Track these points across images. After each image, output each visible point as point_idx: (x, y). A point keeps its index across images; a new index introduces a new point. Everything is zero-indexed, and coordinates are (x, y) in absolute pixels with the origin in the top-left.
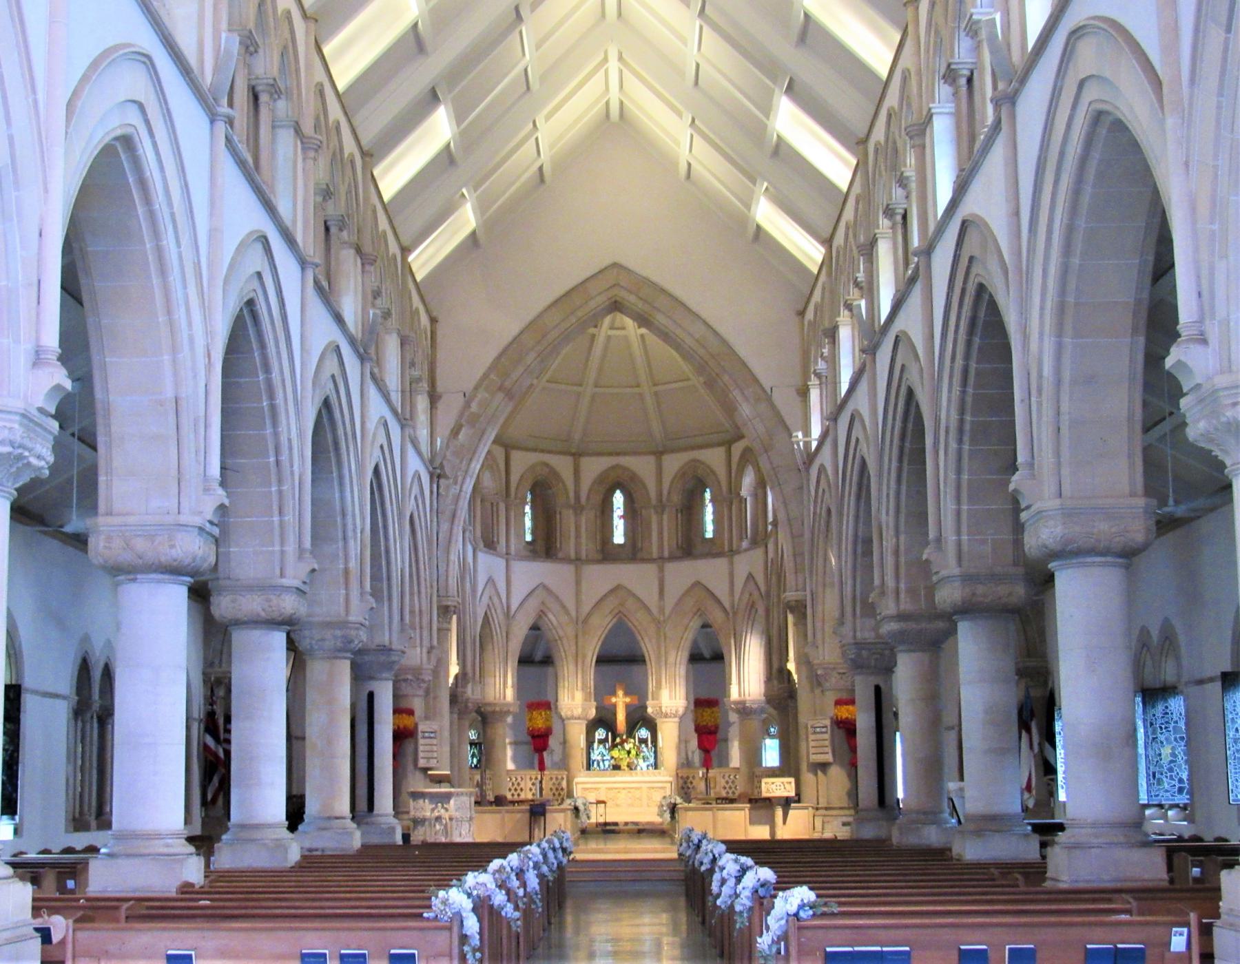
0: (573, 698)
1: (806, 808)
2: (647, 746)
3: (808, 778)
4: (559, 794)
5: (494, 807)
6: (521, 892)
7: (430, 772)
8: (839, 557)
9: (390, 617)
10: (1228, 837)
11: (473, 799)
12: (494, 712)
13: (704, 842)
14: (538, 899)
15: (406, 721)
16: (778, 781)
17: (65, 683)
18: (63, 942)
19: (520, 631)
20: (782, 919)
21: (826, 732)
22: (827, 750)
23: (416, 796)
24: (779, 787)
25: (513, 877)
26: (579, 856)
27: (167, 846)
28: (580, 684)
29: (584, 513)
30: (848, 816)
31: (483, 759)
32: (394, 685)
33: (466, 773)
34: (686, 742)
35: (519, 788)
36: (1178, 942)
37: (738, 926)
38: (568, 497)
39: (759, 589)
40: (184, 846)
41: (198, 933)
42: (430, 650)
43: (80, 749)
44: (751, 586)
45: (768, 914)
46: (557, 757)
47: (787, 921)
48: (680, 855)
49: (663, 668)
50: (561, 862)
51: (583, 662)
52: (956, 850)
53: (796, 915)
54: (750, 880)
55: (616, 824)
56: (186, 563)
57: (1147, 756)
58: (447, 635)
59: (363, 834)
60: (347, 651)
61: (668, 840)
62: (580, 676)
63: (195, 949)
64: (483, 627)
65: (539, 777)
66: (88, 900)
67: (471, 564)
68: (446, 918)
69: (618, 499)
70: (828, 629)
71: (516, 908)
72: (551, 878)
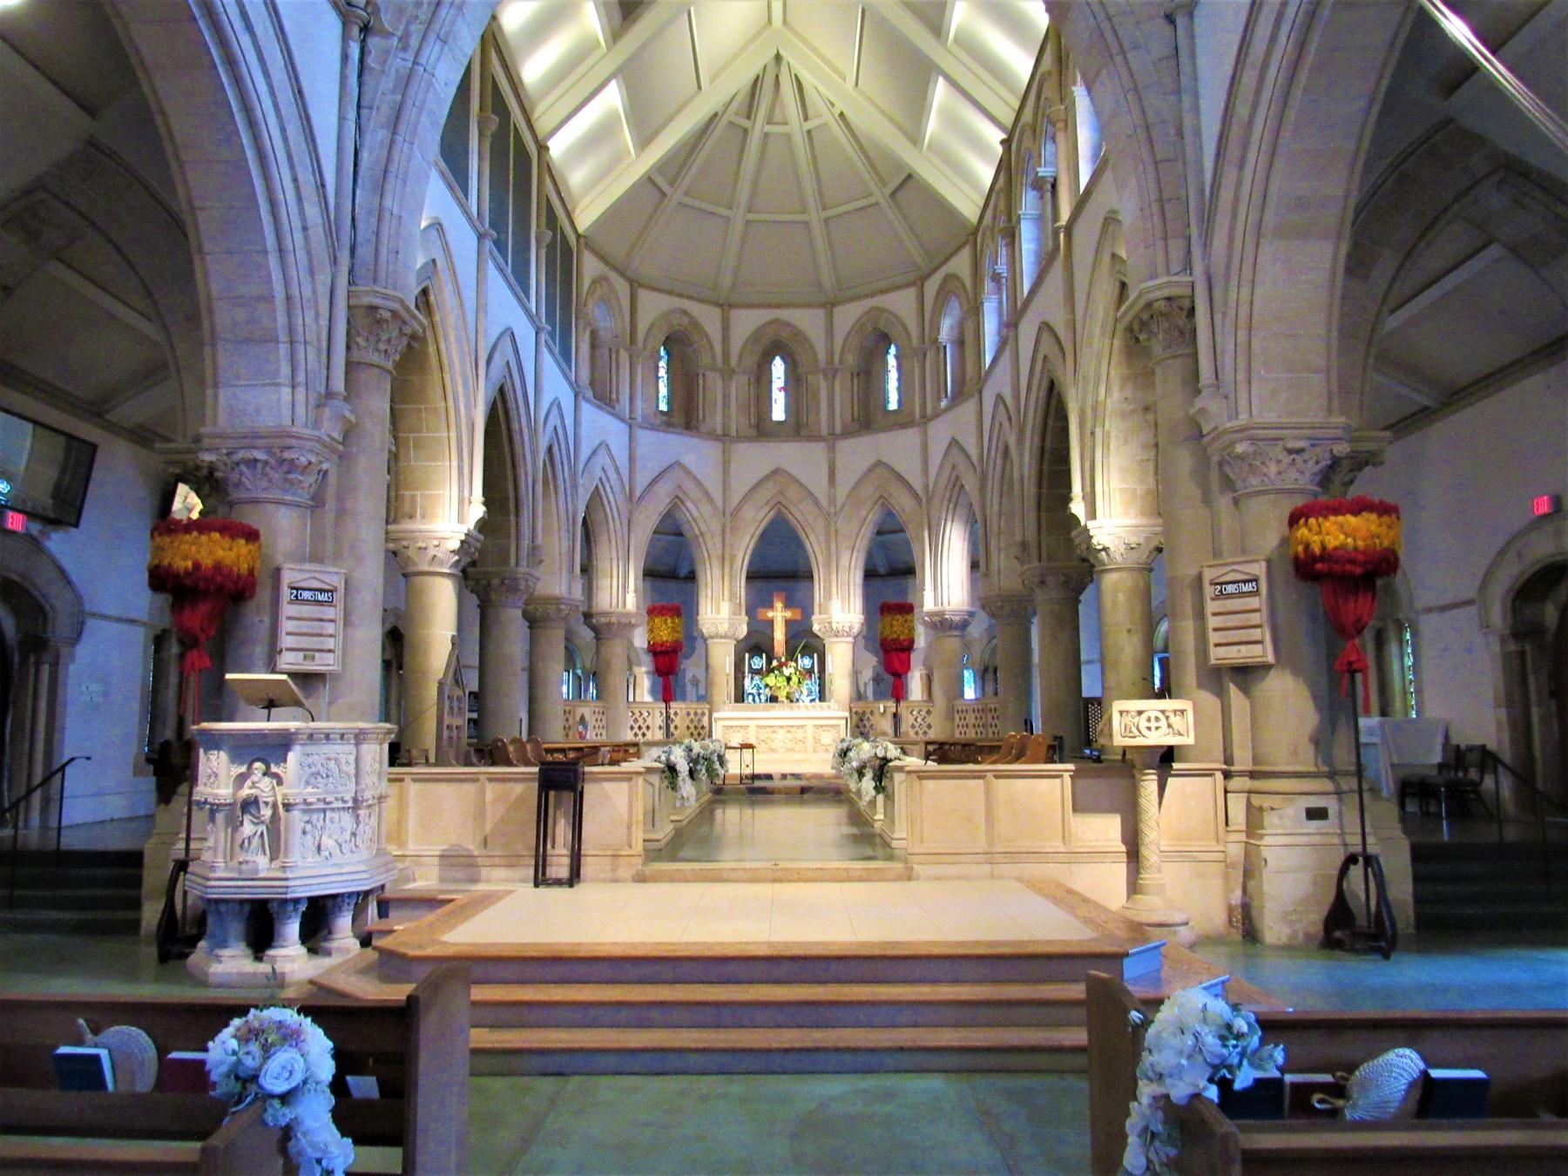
0: (718, 612)
12: (609, 625)
21: (1256, 593)
22: (1256, 634)
28: (726, 593)
29: (735, 378)
38: (713, 356)
39: (968, 457)
51: (731, 567)
55: (769, 777)
69: (778, 367)
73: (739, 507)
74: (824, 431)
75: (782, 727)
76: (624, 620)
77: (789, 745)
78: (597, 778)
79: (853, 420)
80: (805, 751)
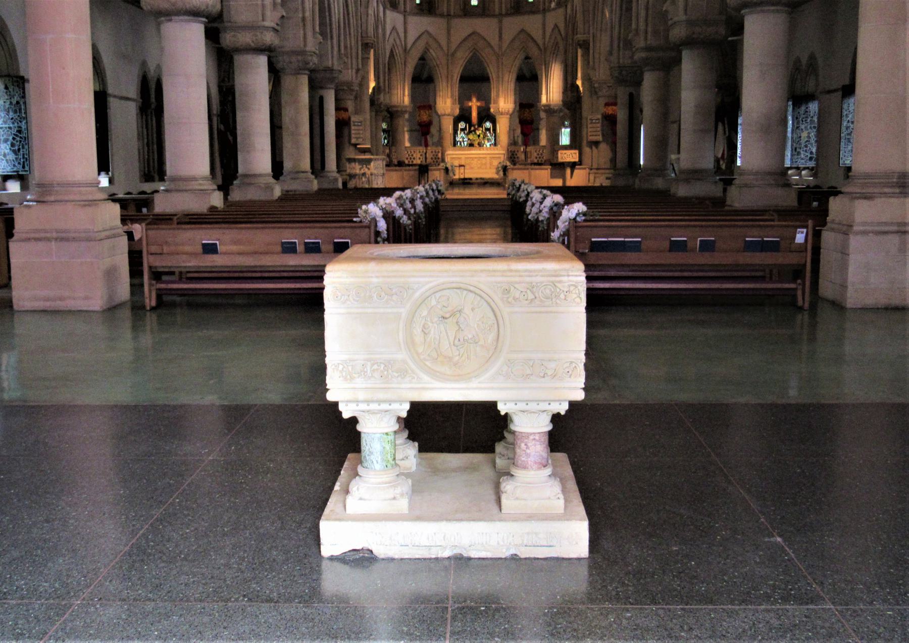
0: (445, 103)
1: (585, 169)
2: (490, 132)
3: (587, 150)
4: (437, 162)
5: (397, 168)
6: (412, 211)
7: (358, 146)
8: (611, 12)
9: (332, 47)
10: (837, 186)
11: (384, 163)
12: (397, 111)
13: (523, 185)
14: (423, 216)
15: (344, 115)
16: (569, 152)
17: (133, 91)
18: (140, 240)
19: (415, 56)
20: (566, 222)
23: (351, 160)
24: (571, 156)
25: (408, 202)
26: (448, 197)
27: (200, 184)
28: (449, 94)
30: (609, 173)
31: (391, 140)
32: (335, 92)
33: (381, 150)
34: (514, 130)
35: (412, 158)
36: (800, 238)
37: (540, 229)
40: (211, 184)
41: (221, 231)
42: (358, 70)
43: (145, 133)
44: (556, 31)
45: (558, 219)
46: (435, 139)
47: (569, 223)
48: (508, 194)
49: (501, 86)
50: (437, 198)
52: (673, 191)
53: (575, 219)
54: (548, 202)
55: (471, 179)
56: (203, 9)
57: (792, 138)
58: (368, 62)
59: (318, 183)
60: (304, 69)
61: (502, 188)
62: (449, 89)
63: (218, 240)
64: (390, 58)
65: (425, 151)
66: (153, 215)
67: (382, 16)
68: (367, 221)
70: (602, 59)
71: (409, 219)
72: (430, 206)
73: (455, 51)
74: (497, 11)
75: (476, 158)
76: (403, 109)
77: (479, 166)
78: (431, 170)
79: (511, 7)
80: (486, 168)
